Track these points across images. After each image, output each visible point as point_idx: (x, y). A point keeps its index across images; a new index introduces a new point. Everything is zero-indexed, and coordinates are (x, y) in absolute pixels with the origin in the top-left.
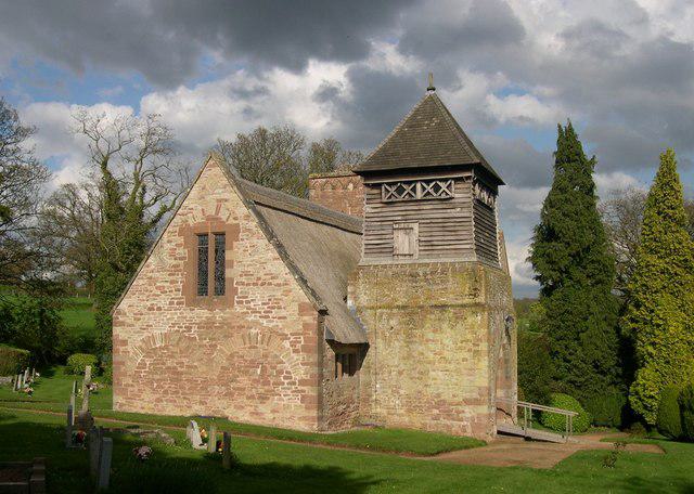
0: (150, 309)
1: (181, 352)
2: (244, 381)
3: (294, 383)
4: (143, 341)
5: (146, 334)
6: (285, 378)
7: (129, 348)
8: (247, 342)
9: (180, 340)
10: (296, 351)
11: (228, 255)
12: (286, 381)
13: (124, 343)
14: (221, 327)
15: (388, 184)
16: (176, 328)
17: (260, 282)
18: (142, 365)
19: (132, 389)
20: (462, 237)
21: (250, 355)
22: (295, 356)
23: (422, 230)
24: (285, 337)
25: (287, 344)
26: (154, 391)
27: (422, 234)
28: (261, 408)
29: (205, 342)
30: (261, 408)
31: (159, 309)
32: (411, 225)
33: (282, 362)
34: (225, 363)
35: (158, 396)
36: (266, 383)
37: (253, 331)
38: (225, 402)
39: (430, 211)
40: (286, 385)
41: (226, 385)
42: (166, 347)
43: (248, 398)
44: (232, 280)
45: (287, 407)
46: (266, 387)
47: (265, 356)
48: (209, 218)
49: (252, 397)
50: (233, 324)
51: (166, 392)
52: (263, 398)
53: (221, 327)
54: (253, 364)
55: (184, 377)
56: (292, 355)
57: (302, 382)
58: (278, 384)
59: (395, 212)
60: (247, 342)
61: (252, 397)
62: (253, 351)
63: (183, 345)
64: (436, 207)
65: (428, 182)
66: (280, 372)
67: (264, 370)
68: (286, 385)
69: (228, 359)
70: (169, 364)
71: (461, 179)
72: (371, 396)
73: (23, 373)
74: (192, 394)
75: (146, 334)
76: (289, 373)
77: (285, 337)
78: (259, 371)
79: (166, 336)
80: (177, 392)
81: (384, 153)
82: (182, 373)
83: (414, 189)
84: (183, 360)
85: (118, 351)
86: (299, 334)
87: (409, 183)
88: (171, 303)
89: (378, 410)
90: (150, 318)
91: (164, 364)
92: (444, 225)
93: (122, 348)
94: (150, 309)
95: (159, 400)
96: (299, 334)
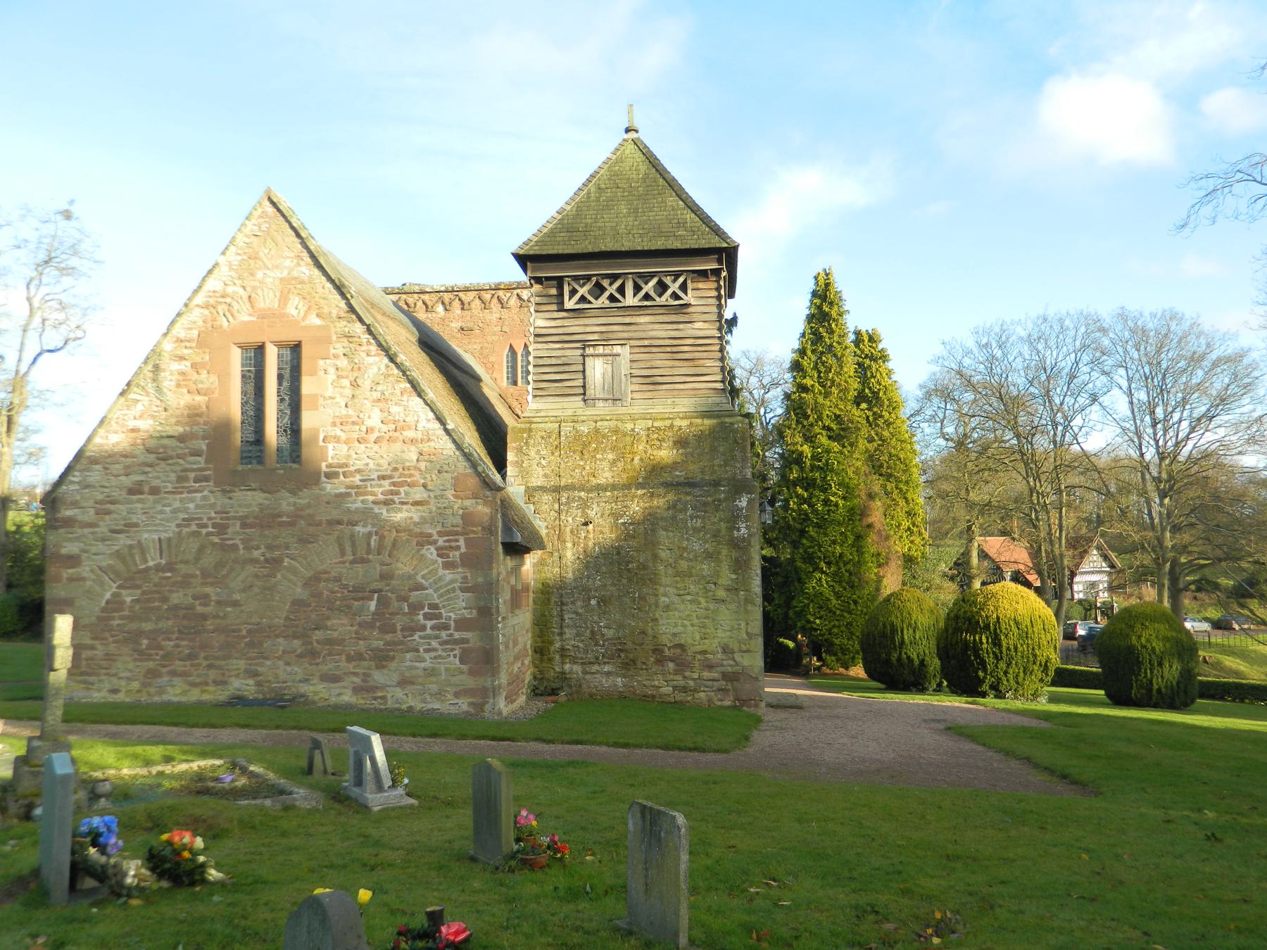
0: (131, 492)
1: (205, 574)
2: (340, 626)
3: (446, 627)
4: (118, 555)
5: (123, 541)
6: (426, 617)
7: (85, 570)
8: (348, 549)
9: (201, 550)
10: (447, 566)
11: (308, 386)
12: (429, 624)
13: (73, 560)
14: (292, 524)
15: (576, 278)
16: (194, 528)
17: (373, 437)
18: (115, 604)
19: (89, 653)
20: (705, 371)
21: (357, 574)
22: (448, 575)
23: (636, 357)
24: (425, 540)
25: (431, 552)
26: (142, 655)
27: (635, 365)
28: (379, 677)
29: (256, 554)
30: (379, 677)
31: (155, 491)
32: (617, 349)
33: (420, 587)
34: (300, 592)
35: (151, 664)
36: (388, 629)
37: (360, 530)
38: (298, 670)
39: (652, 327)
40: (429, 631)
41: (304, 636)
42: (170, 567)
43: (350, 659)
44: (316, 437)
45: (431, 673)
46: (388, 637)
47: (384, 577)
48: (263, 315)
49: (359, 657)
50: (318, 518)
51: (168, 656)
52: (382, 658)
53: (292, 524)
54: (361, 593)
55: (209, 625)
56: (441, 572)
57: (462, 624)
58: (413, 629)
59: (588, 326)
60: (348, 549)
61: (359, 657)
62: (359, 568)
63: (209, 560)
64: (661, 318)
65: (647, 277)
66: (415, 608)
67: (383, 602)
68: (429, 631)
69: (306, 585)
70: (176, 598)
71: (703, 274)
72: (551, 643)
73: (732, 424)
74: (225, 658)
75: (123, 541)
76: (435, 607)
77: (425, 540)
78: (373, 605)
79: (164, 546)
80: (191, 657)
81: (566, 224)
82: (204, 617)
83: (621, 290)
84: (208, 590)
85: (58, 579)
86: (457, 534)
87: (614, 278)
88: (181, 479)
89: (567, 667)
90: (137, 509)
91: (165, 599)
92: (673, 349)
93: (67, 573)
94: (131, 492)
95: (154, 674)
96: (457, 534)
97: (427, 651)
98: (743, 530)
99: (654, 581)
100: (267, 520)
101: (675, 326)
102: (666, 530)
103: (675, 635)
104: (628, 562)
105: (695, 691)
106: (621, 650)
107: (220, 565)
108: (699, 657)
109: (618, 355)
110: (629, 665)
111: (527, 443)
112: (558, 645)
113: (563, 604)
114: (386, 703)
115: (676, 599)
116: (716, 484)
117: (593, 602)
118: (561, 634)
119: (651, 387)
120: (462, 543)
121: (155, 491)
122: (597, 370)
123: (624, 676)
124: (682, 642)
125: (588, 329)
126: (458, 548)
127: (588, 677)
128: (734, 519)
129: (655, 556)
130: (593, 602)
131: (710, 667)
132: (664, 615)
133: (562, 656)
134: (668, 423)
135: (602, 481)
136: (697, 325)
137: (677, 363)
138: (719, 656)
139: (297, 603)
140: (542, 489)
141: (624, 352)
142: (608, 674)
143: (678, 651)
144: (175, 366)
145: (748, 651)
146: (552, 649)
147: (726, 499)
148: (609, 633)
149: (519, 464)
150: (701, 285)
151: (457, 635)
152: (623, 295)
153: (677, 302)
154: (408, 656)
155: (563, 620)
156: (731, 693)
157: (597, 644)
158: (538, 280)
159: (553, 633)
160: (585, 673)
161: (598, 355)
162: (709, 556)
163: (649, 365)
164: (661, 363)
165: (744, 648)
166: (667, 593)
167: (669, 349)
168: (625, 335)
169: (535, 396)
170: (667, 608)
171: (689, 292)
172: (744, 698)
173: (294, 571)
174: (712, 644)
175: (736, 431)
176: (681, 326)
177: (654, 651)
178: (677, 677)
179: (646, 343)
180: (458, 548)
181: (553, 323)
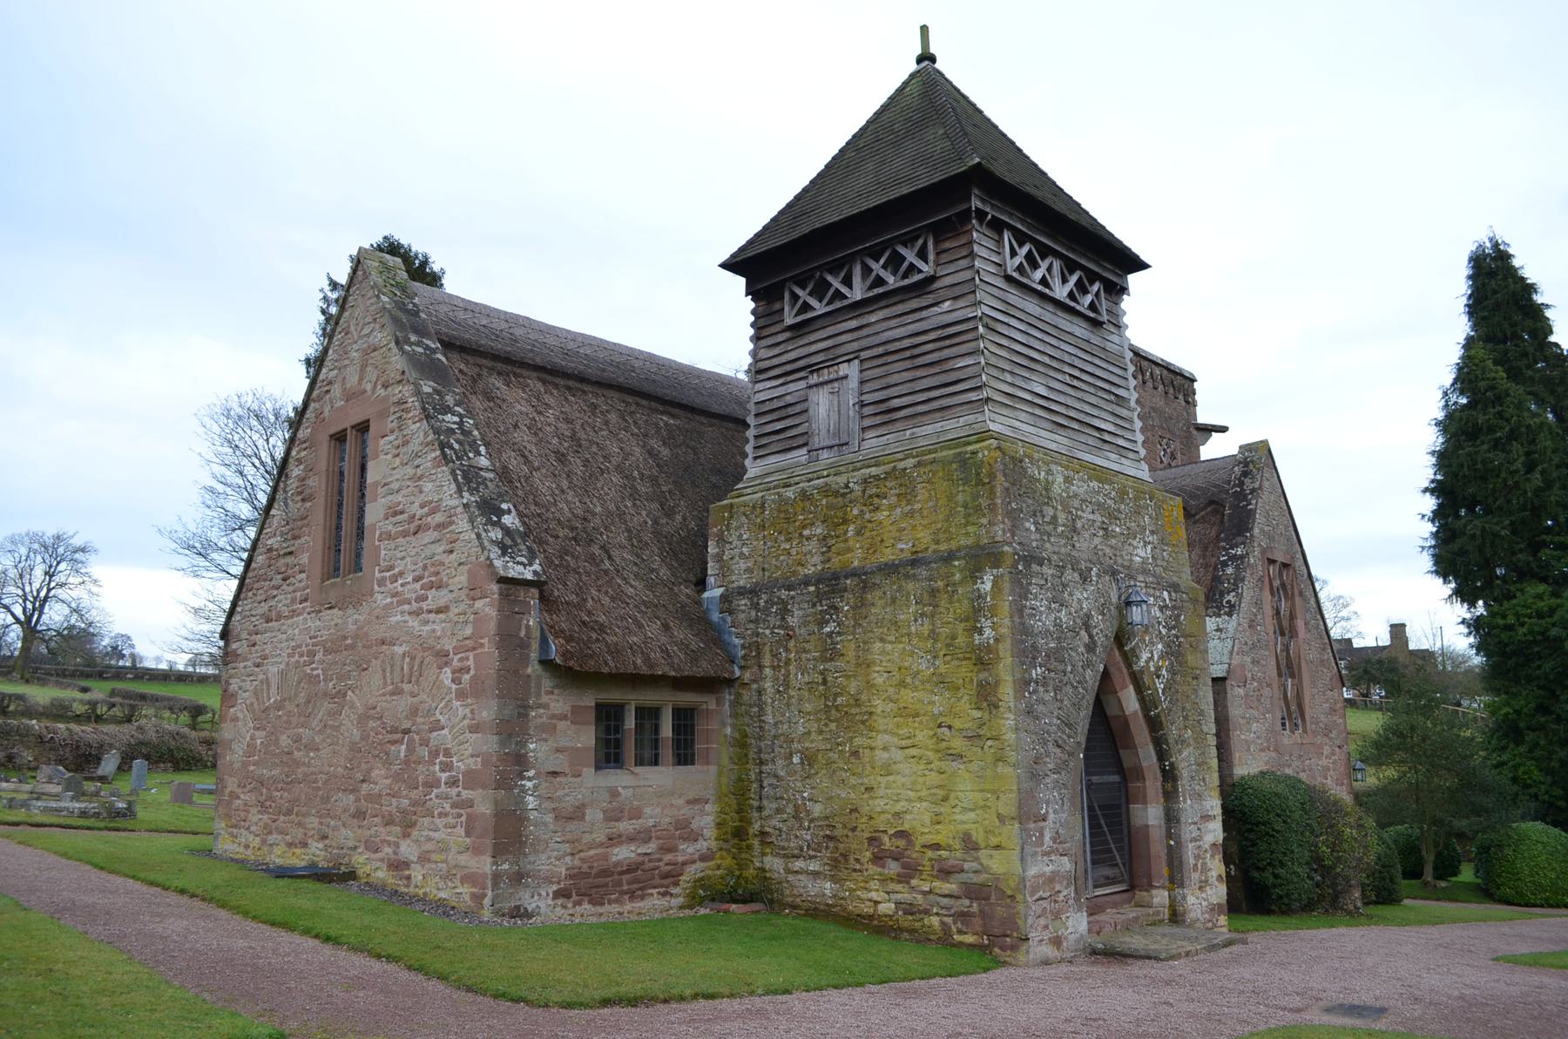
10: (461, 695)
12: (444, 776)
24: (443, 657)
25: (447, 675)
32: (844, 369)
57: (471, 779)
64: (900, 308)
73: (974, 453)
89: (768, 859)
97: (440, 815)
98: (988, 632)
99: (866, 721)
101: (917, 316)
102: (882, 640)
103: (897, 815)
104: (836, 695)
105: (927, 912)
106: (830, 838)
108: (930, 853)
109: (846, 377)
110: (840, 863)
111: (728, 526)
112: (757, 826)
113: (762, 763)
114: (407, 886)
115: (898, 755)
116: (949, 557)
117: (796, 760)
118: (760, 809)
119: (886, 418)
120: (471, 662)
122: (822, 405)
123: (834, 879)
124: (906, 827)
125: (813, 348)
126: (468, 670)
127: (791, 878)
128: (976, 612)
129: (870, 685)
130: (796, 760)
131: (945, 873)
132: (883, 780)
133: (763, 843)
134: (888, 467)
135: (810, 570)
136: (947, 305)
137: (919, 373)
138: (958, 854)
140: (742, 592)
141: (851, 370)
142: (816, 874)
143: (902, 843)
145: (998, 847)
146: (751, 831)
147: (961, 582)
148: (817, 810)
149: (719, 558)
150: (947, 245)
151: (466, 794)
152: (850, 287)
153: (1092, 315)
154: (426, 820)
155: (762, 787)
156: (977, 921)
157: (801, 827)
159: (751, 807)
160: (788, 871)
161: (822, 384)
162: (942, 682)
163: (884, 382)
164: (898, 373)
165: (994, 841)
166: (884, 743)
167: (908, 354)
168: (855, 346)
169: (755, 458)
170: (887, 769)
171: (931, 257)
172: (996, 931)
174: (943, 835)
175: (980, 465)
176: (924, 314)
177: (871, 840)
178: (899, 887)
179: (881, 350)
180: (468, 670)
181: (777, 351)
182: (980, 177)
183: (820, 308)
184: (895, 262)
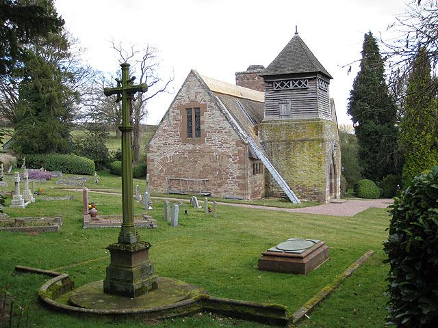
10: (235, 163)
18: (162, 171)
21: (214, 165)
24: (230, 157)
31: (169, 144)
32: (288, 101)
42: (173, 162)
52: (220, 185)
54: (215, 169)
57: (238, 178)
63: (181, 161)
70: (175, 169)
83: (289, 84)
100: (193, 151)
107: (183, 162)
121: (169, 144)
139: (200, 171)
144: (172, 114)
158: (266, 82)
173: (200, 164)
182: (320, 73)
183: (282, 88)
184: (300, 84)
